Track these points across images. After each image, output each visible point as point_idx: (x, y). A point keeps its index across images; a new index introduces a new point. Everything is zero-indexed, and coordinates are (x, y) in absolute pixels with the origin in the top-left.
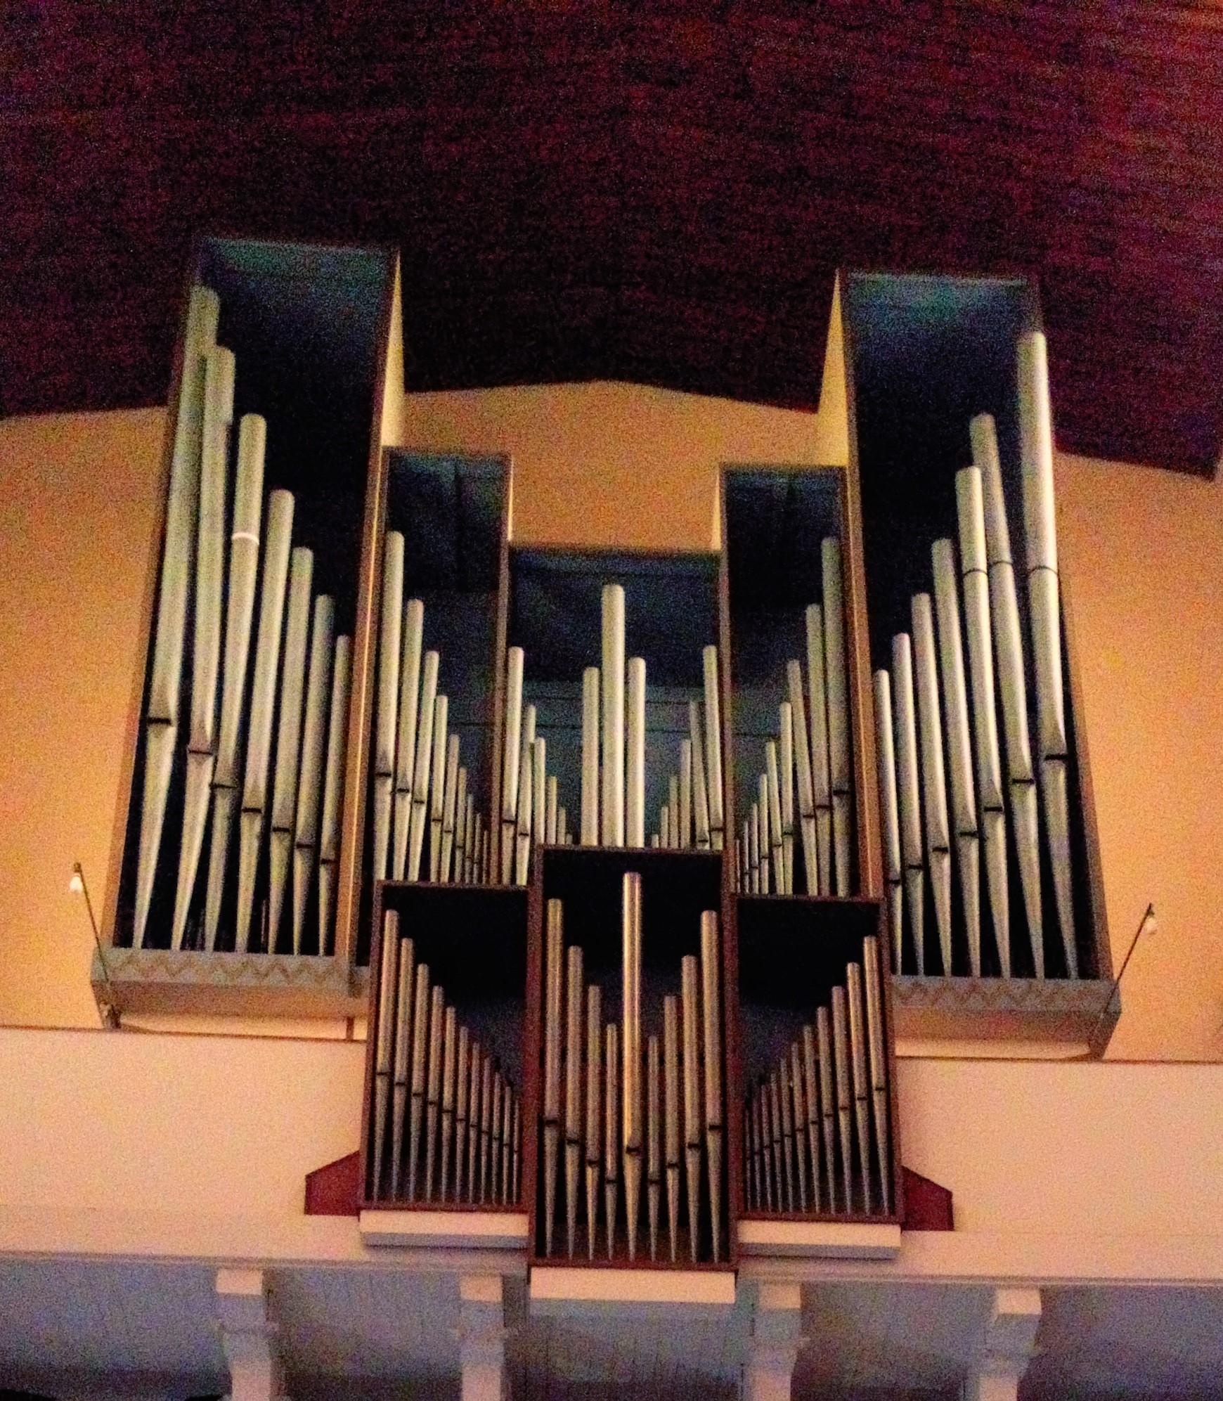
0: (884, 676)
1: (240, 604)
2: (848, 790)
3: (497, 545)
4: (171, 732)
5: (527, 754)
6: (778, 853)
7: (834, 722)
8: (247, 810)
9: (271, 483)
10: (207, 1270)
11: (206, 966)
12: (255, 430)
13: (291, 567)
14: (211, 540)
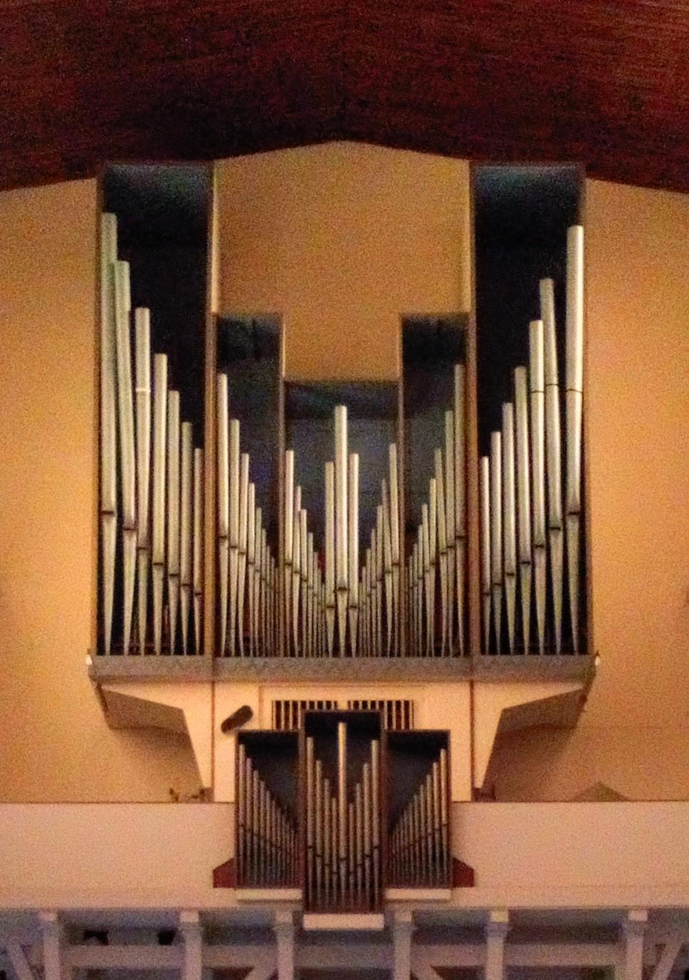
0: (486, 460)
1: (143, 434)
2: (465, 539)
3: (276, 379)
4: (114, 521)
5: (297, 520)
6: (427, 576)
7: (458, 493)
8: (156, 564)
9: (155, 350)
10: (177, 913)
11: (141, 663)
12: (144, 316)
13: (169, 402)
14: (126, 396)
